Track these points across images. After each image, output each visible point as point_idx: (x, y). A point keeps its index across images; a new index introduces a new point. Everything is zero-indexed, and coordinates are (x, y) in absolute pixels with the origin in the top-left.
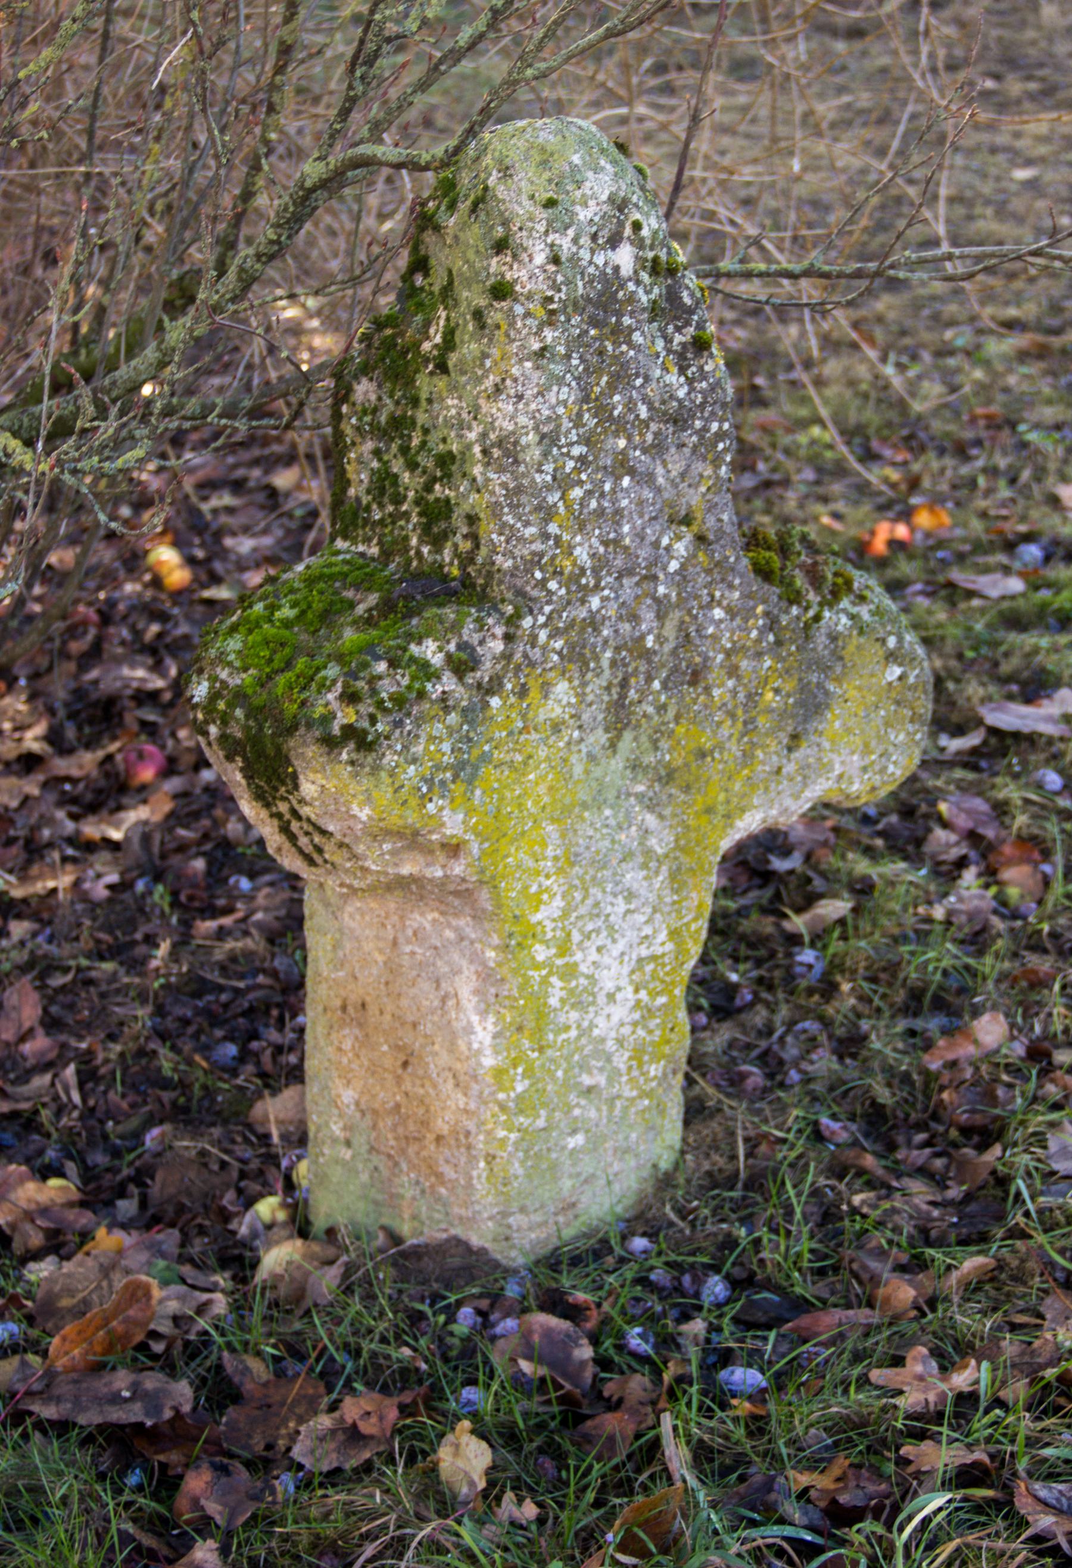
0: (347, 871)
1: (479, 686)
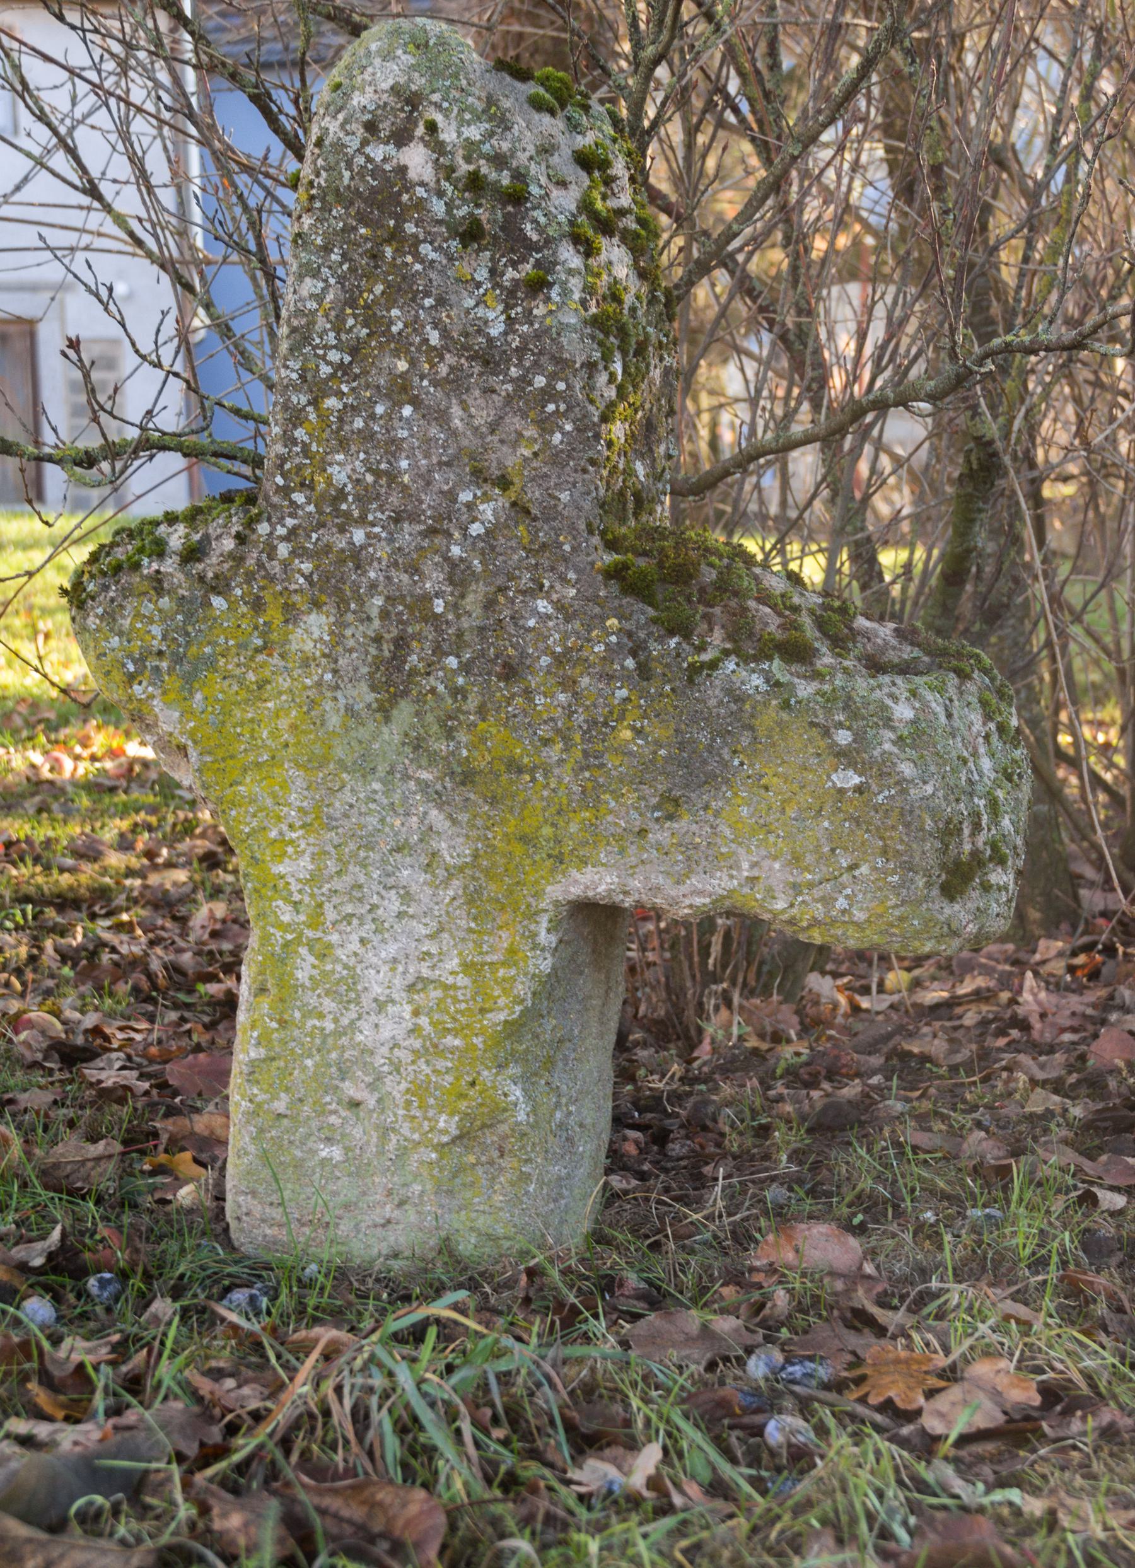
1: (201, 578)
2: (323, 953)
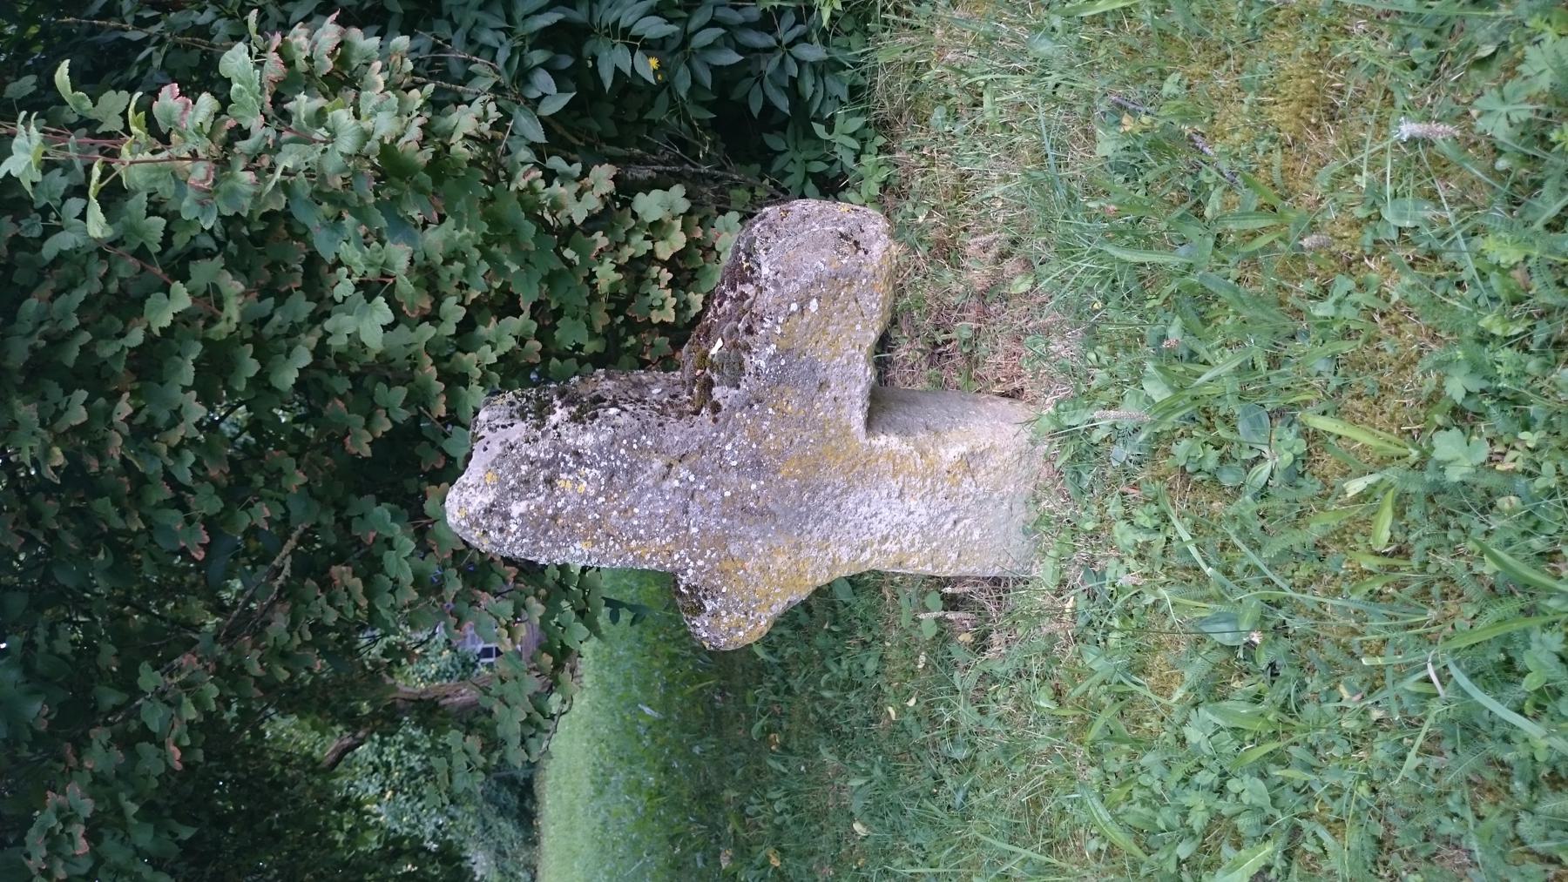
2: (885, 539)
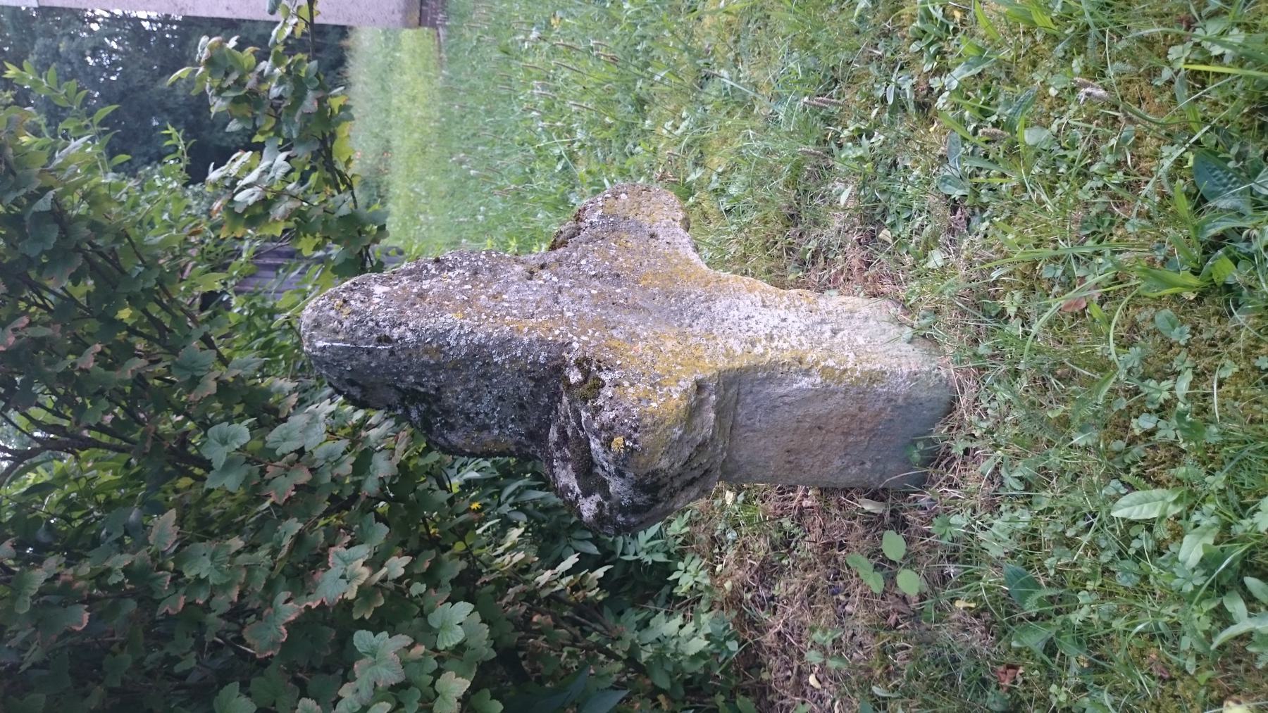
0: (714, 451)
